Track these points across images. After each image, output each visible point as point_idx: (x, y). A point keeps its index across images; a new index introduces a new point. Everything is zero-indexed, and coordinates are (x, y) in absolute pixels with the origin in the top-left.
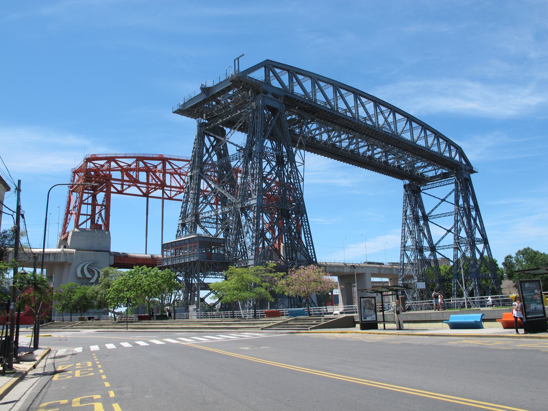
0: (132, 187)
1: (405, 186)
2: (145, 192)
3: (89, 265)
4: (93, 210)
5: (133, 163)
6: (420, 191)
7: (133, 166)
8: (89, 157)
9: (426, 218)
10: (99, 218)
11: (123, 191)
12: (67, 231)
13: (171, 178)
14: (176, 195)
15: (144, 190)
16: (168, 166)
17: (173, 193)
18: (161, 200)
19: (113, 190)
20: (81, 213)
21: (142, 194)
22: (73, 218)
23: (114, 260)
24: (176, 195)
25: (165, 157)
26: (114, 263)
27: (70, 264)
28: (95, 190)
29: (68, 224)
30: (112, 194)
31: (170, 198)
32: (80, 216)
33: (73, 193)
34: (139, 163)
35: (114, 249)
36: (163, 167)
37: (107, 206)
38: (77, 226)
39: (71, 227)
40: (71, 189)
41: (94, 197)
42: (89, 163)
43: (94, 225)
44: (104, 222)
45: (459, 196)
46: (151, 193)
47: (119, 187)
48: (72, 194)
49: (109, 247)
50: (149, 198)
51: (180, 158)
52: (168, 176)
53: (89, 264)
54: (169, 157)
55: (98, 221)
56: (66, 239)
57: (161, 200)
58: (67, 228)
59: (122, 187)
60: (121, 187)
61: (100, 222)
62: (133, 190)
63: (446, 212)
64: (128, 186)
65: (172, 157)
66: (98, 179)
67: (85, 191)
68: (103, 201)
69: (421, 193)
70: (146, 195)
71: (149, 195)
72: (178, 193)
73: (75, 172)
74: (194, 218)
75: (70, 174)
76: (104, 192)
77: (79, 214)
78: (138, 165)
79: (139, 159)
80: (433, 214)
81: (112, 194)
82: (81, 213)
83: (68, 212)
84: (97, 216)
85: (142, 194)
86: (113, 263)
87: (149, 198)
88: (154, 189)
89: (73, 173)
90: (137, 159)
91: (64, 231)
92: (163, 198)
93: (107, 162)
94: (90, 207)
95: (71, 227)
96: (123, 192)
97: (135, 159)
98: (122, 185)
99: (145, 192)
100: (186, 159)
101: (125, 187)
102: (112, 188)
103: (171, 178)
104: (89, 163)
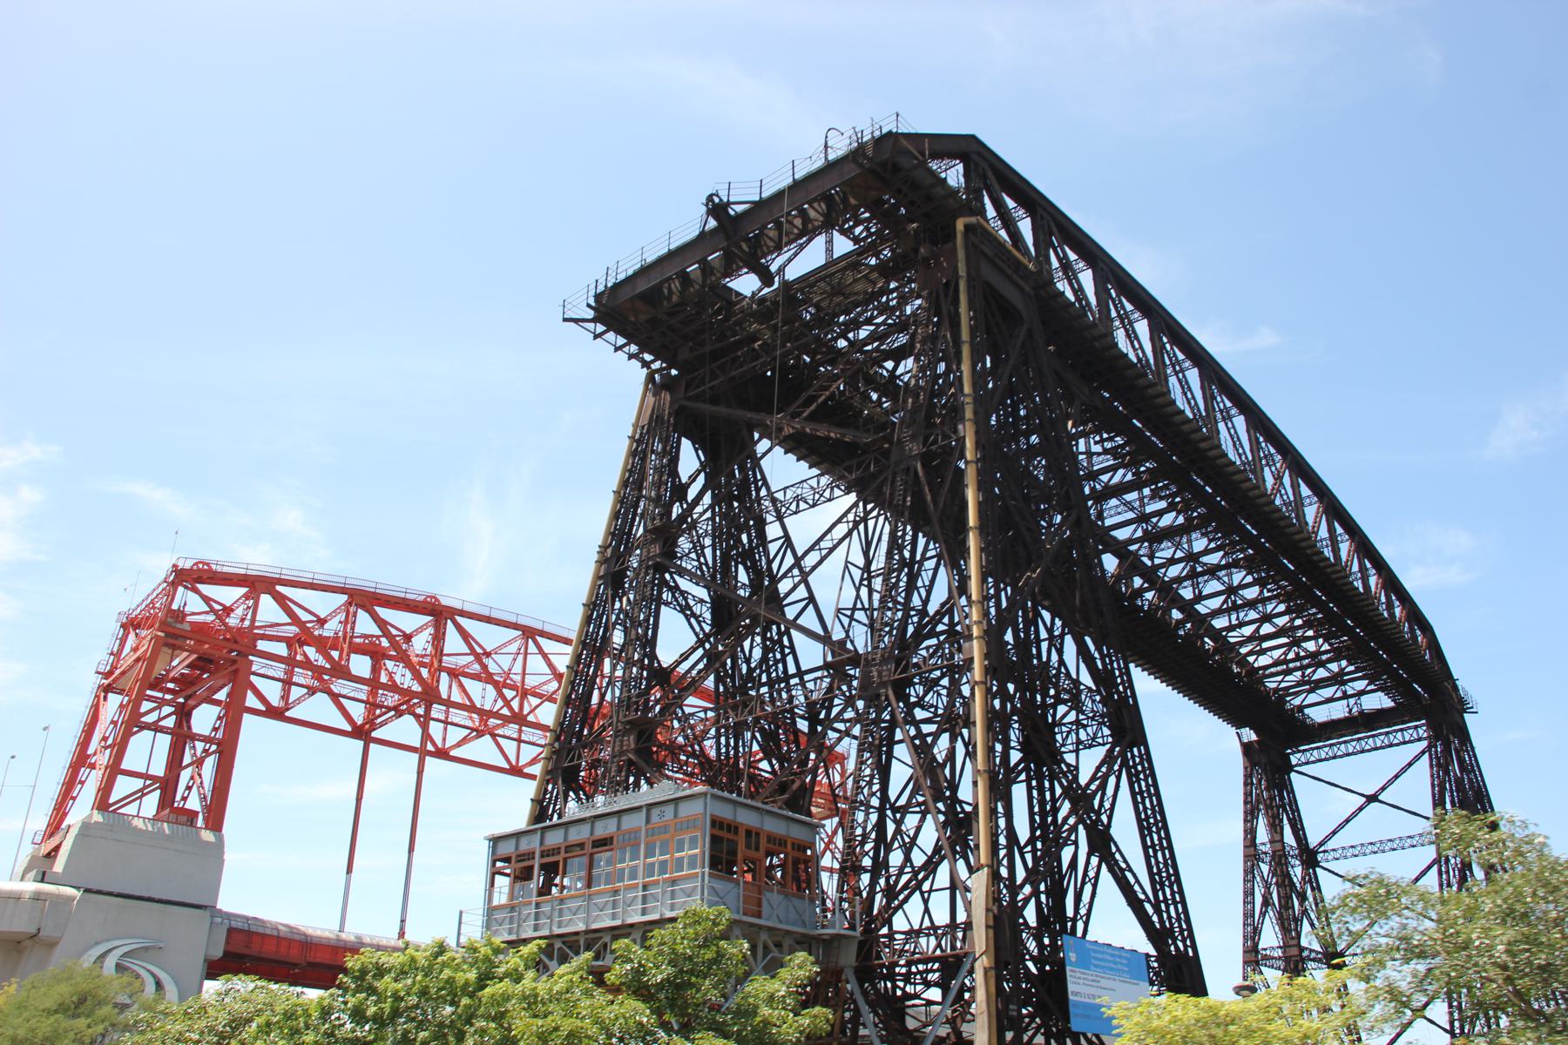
0: (319, 694)
1: (1247, 748)
2: (360, 721)
3: (125, 955)
4: (175, 763)
5: (335, 613)
6: (1290, 768)
7: (332, 628)
8: (188, 565)
9: (1310, 858)
10: (189, 788)
11: (288, 709)
12: (64, 826)
13: (450, 687)
14: (464, 741)
15: (358, 712)
16: (453, 642)
17: (455, 735)
18: (416, 757)
19: (251, 701)
20: (124, 766)
21: (349, 728)
22: (92, 782)
23: (227, 943)
24: (464, 741)
25: (445, 602)
26: (226, 953)
27: (52, 945)
28: (188, 694)
29: (74, 799)
30: (246, 717)
31: (442, 754)
32: (120, 777)
33: (110, 695)
34: (355, 615)
35: (229, 901)
36: (434, 638)
37: (226, 748)
38: (102, 803)
39: (82, 810)
40: (104, 681)
41: (184, 714)
42: (181, 589)
43: (167, 811)
44: (206, 801)
45: (1281, 821)
46: (382, 724)
47: (273, 692)
48: (105, 698)
49: (216, 903)
50: (372, 745)
51: (495, 615)
52: (444, 677)
53: (126, 949)
54: (457, 605)
55: (185, 799)
56: (52, 855)
57: (416, 757)
58: (65, 814)
59: (285, 696)
60: (282, 697)
61: (194, 803)
62: (319, 708)
63: (1404, 834)
64: (305, 691)
65: (468, 608)
66: (207, 646)
67: (149, 692)
68: (215, 729)
69: (1293, 775)
70: (362, 733)
71: (374, 734)
72: (475, 733)
73: (131, 624)
74: (630, 741)
75: (114, 628)
76: (217, 703)
77: (115, 770)
78: (350, 621)
79: (363, 599)
80: (1330, 845)
81: (246, 717)
82: (124, 766)
83: (81, 760)
84: (185, 776)
85: (349, 728)
86: (221, 955)
87: (372, 745)
88: (393, 713)
89: (123, 626)
90: (351, 596)
91: (55, 825)
92: (422, 753)
93: (247, 597)
94: (164, 741)
95: (82, 810)
96: (287, 714)
97: (344, 598)
98: (288, 683)
99: (360, 721)
100: (512, 619)
101: (296, 692)
102: (250, 694)
103: (450, 687)
104: (181, 589)
